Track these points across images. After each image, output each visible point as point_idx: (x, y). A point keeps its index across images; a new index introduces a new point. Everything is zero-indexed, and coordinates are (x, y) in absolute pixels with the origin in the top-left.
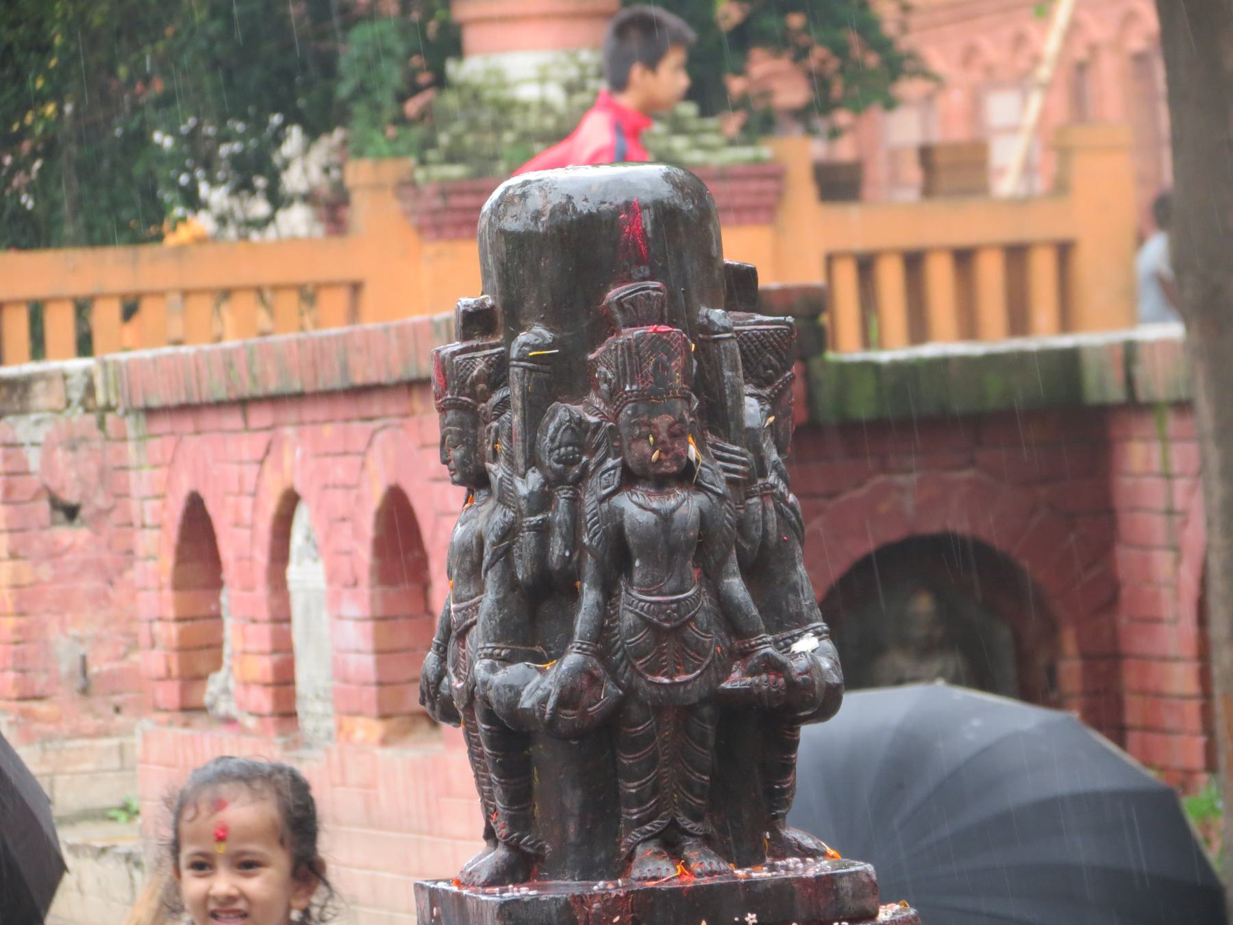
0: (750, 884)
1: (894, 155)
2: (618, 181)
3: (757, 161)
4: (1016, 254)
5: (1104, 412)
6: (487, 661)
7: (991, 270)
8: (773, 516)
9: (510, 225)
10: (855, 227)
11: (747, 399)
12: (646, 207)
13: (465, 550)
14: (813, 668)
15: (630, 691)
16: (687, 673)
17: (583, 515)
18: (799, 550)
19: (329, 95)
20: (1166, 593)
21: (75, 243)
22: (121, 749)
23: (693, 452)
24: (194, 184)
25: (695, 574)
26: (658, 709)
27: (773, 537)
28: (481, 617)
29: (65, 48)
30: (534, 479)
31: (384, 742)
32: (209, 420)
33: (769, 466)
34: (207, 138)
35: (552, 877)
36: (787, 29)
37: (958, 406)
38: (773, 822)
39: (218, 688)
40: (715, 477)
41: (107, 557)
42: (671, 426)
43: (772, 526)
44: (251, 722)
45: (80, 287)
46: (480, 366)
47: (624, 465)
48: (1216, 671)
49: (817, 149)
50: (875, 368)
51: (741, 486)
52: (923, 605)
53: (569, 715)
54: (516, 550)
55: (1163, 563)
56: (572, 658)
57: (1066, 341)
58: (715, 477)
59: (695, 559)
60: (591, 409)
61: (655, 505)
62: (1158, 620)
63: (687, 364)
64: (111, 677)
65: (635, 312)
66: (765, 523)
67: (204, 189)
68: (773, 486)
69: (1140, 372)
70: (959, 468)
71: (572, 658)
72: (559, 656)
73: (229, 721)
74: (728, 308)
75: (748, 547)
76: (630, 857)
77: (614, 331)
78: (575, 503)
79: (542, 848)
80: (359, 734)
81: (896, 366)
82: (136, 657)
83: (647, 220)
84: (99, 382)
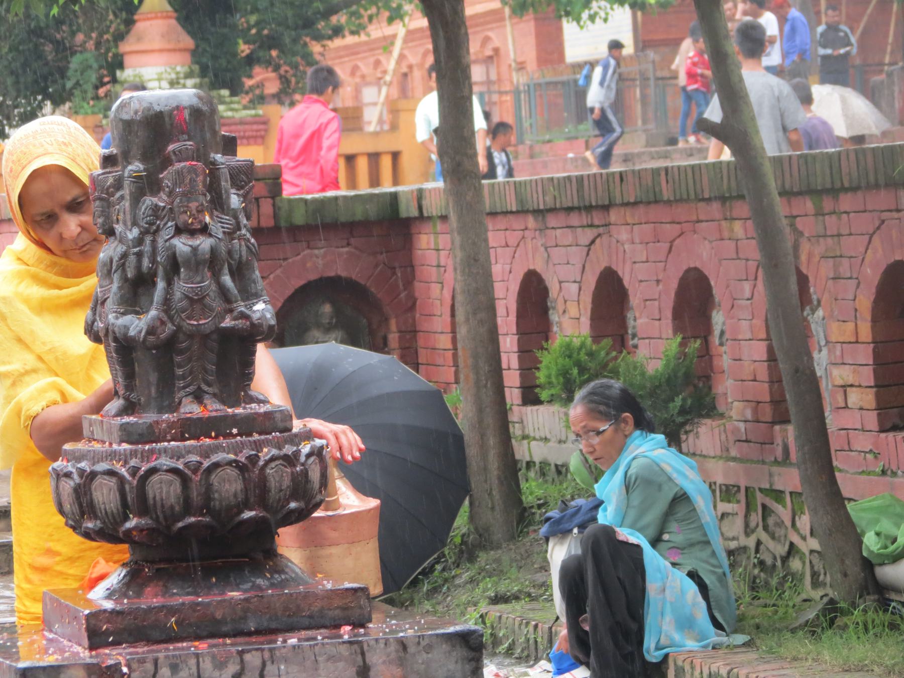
0: (234, 415)
2: (174, 97)
3: (256, 116)
4: (374, 158)
6: (114, 314)
7: (362, 165)
8: (244, 248)
9: (126, 117)
11: (232, 196)
12: (186, 108)
13: (105, 265)
14: (263, 317)
15: (179, 328)
18: (256, 264)
19: (64, 86)
23: (208, 219)
25: (209, 274)
26: (191, 336)
27: (244, 258)
28: (111, 295)
30: (135, 232)
34: (8, 106)
35: (144, 413)
36: (271, 56)
37: (343, 219)
40: (217, 230)
42: (197, 207)
43: (244, 253)
46: (111, 181)
47: (176, 225)
48: (458, 336)
50: (306, 201)
52: (327, 308)
53: (151, 338)
54: (127, 264)
55: (435, 289)
56: (153, 313)
58: (217, 230)
59: (209, 268)
60: (161, 200)
61: (190, 243)
63: (205, 180)
65: (181, 156)
71: (153, 313)
72: (147, 312)
74: (224, 154)
75: (233, 262)
76: (180, 403)
78: (154, 242)
79: (139, 400)
81: (314, 201)
83: (186, 114)
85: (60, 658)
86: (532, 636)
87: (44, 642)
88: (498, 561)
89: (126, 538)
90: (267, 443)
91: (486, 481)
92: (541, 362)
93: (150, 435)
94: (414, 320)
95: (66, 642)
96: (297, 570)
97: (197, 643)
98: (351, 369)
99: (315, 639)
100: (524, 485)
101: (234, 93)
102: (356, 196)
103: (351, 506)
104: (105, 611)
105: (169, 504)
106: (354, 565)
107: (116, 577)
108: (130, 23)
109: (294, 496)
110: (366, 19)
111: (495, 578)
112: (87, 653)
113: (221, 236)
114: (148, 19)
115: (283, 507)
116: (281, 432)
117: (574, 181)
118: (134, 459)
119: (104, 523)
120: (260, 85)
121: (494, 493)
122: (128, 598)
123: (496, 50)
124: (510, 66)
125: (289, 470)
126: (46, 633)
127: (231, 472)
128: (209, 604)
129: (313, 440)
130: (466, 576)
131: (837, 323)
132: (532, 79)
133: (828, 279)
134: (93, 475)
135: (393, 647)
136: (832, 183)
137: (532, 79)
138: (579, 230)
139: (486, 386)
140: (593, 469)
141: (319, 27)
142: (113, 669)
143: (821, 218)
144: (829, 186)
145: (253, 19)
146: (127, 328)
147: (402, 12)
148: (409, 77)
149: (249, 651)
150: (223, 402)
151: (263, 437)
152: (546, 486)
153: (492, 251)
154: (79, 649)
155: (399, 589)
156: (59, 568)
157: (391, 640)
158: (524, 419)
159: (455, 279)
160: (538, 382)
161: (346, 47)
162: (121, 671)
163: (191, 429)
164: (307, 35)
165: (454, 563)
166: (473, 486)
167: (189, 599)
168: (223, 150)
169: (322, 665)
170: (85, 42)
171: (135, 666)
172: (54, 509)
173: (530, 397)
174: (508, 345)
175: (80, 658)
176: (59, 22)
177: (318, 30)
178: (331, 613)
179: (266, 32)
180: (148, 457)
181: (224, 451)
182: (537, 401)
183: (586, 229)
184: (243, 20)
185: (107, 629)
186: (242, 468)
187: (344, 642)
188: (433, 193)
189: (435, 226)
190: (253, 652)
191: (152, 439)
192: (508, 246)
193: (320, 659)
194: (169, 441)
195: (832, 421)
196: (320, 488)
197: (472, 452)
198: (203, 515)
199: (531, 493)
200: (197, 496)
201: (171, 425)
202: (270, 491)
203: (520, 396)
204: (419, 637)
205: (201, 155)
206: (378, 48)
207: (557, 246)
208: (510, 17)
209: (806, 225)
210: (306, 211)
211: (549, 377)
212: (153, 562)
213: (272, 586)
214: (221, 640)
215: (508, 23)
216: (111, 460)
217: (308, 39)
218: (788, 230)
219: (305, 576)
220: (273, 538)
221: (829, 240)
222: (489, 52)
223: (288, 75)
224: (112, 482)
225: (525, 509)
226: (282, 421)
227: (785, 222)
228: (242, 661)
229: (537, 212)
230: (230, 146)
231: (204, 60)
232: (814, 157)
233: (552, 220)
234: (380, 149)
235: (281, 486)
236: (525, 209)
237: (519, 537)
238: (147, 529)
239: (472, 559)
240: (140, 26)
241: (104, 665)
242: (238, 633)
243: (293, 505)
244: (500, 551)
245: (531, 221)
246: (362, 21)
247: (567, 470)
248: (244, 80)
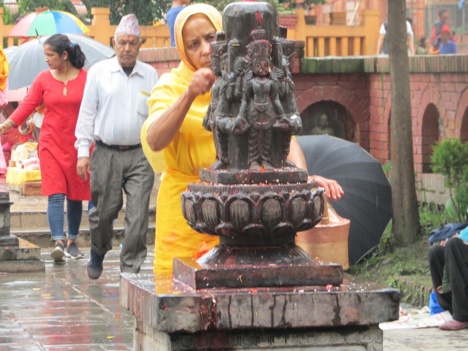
1: (324, 15)
2: (256, 6)
3: (292, 14)
4: (351, 39)
5: (369, 74)
7: (345, 42)
8: (288, 87)
9: (230, 15)
10: (313, 31)
14: (295, 123)
15: (252, 126)
17: (243, 83)
20: (381, 117)
23: (270, 70)
24: (160, 12)
26: (258, 130)
27: (287, 92)
28: (218, 107)
33: (287, 75)
37: (335, 71)
40: (275, 76)
43: (288, 89)
46: (221, 48)
48: (392, 136)
49: (306, 12)
50: (316, 61)
51: (281, 79)
52: (324, 117)
53: (237, 130)
54: (227, 91)
55: (381, 110)
56: (239, 117)
57: (361, 57)
58: (275, 76)
59: (269, 96)
60: (246, 59)
62: (379, 123)
65: (258, 37)
66: (286, 88)
67: (162, 14)
69: (378, 65)
70: (334, 85)
72: (236, 116)
74: (280, 37)
75: (281, 93)
76: (250, 164)
78: (241, 81)
81: (320, 61)
83: (262, 15)
85: (181, 293)
86: (421, 293)
87: (173, 284)
88: (405, 253)
89: (219, 233)
91: (401, 211)
93: (234, 180)
94: (369, 125)
95: (184, 285)
96: (306, 255)
97: (252, 289)
98: (335, 149)
99: (313, 291)
100: (421, 215)
103: (335, 223)
104: (205, 270)
105: (242, 216)
106: (335, 254)
107: (212, 252)
111: (403, 262)
112: (195, 291)
113: (276, 79)
115: (300, 221)
116: (301, 182)
117: (456, 59)
118: (225, 192)
119: (207, 224)
122: (218, 263)
125: (304, 203)
126: (174, 279)
127: (275, 202)
128: (260, 269)
129: (318, 188)
130: (388, 260)
134: (203, 199)
135: (353, 298)
140: (458, 208)
142: (208, 300)
146: (225, 124)
149: (279, 295)
150: (273, 166)
151: (292, 185)
153: (411, 93)
154: (190, 288)
156: (178, 243)
157: (352, 294)
158: (423, 180)
160: (431, 162)
162: (212, 301)
163: (255, 178)
166: (395, 213)
167: (249, 266)
169: (316, 305)
171: (219, 299)
172: (182, 217)
173: (427, 169)
175: (191, 293)
178: (322, 278)
180: (232, 192)
181: (272, 191)
182: (430, 171)
185: (206, 279)
186: (281, 200)
187: (328, 294)
190: (281, 296)
191: (235, 182)
193: (315, 302)
194: (243, 184)
197: (395, 196)
198: (258, 223)
201: (245, 176)
202: (294, 213)
204: (367, 293)
205: (268, 36)
210: (316, 66)
211: (437, 159)
212: (231, 246)
213: (293, 262)
214: (264, 289)
216: (213, 192)
219: (309, 258)
224: (213, 204)
225: (421, 227)
226: (302, 177)
228: (275, 300)
230: (283, 33)
233: (443, 78)
235: (300, 210)
239: (392, 251)
241: (203, 298)
242: (274, 286)
243: (305, 221)
244: (406, 248)
245: (432, 78)
247: (444, 208)
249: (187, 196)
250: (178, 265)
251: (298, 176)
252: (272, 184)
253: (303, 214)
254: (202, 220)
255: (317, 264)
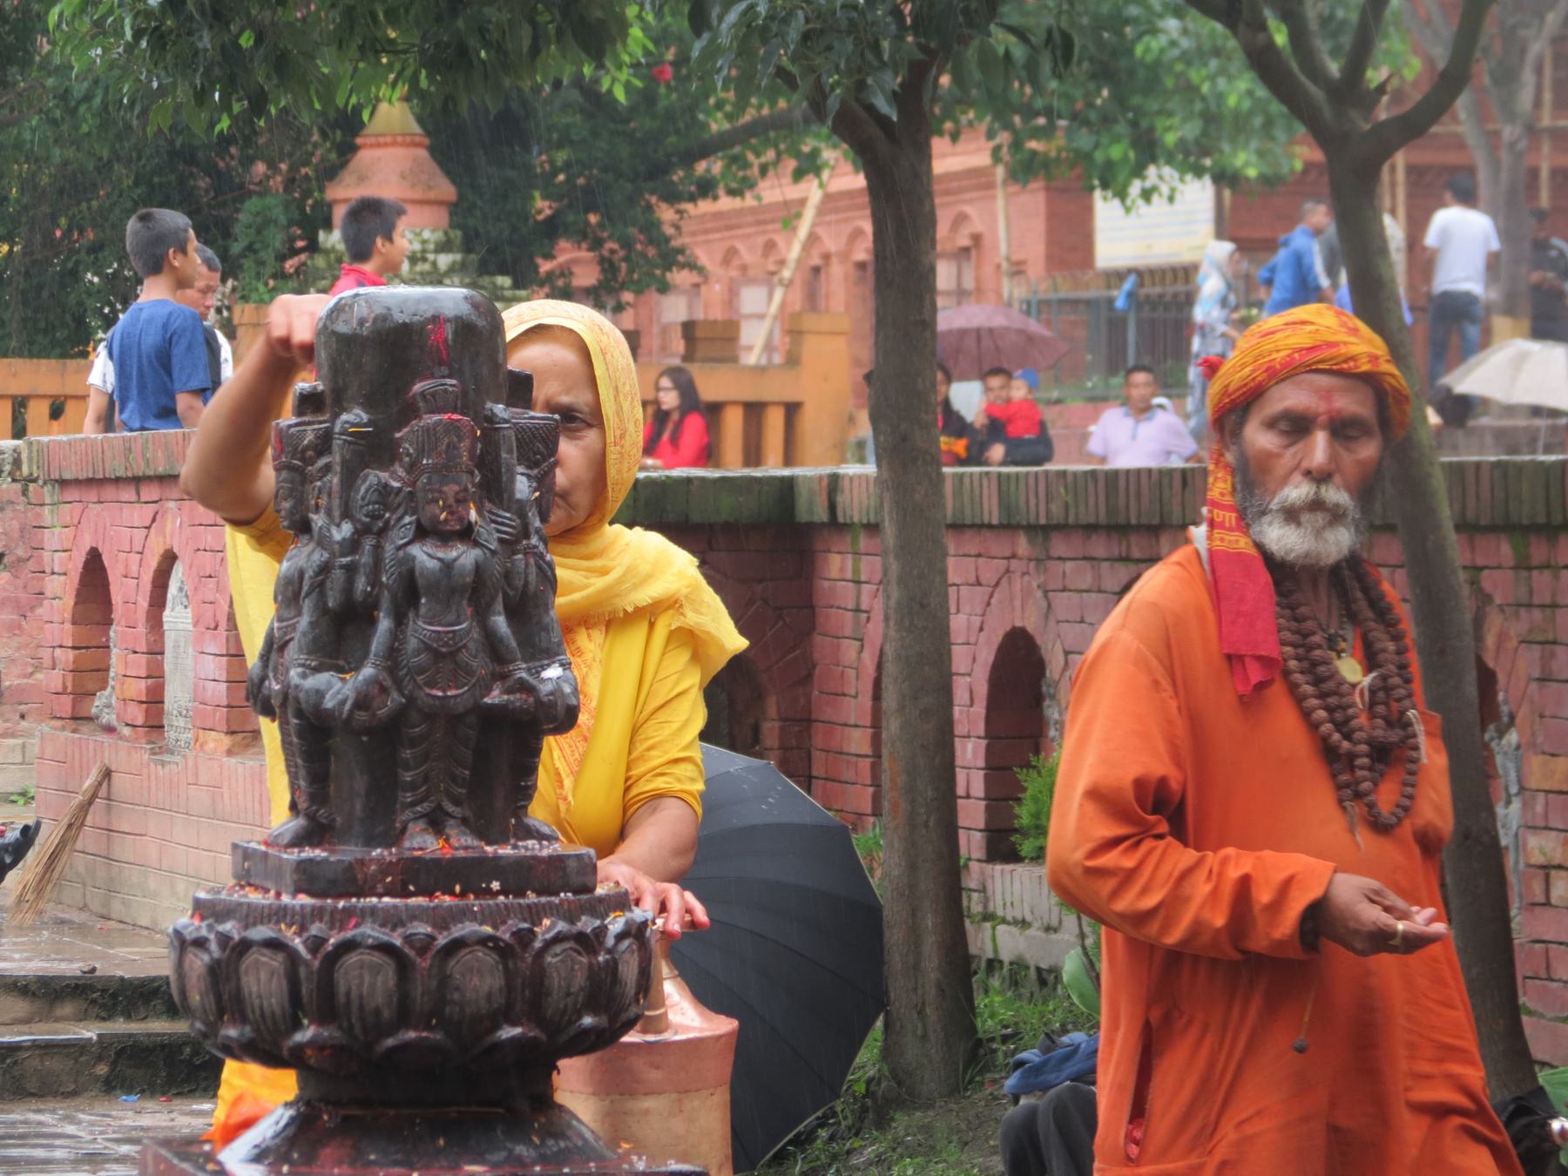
1: (665, 330)
2: (429, 299)
4: (754, 411)
5: (811, 527)
6: (300, 670)
8: (533, 570)
9: (342, 328)
12: (449, 320)
15: (411, 700)
16: (458, 688)
21: (18, 353)
22: (24, 746)
23: (473, 515)
25: (469, 611)
26: (430, 716)
27: (532, 587)
28: (297, 635)
29: (18, 201)
30: (347, 529)
31: (230, 753)
32: (110, 492)
33: (532, 531)
34: (126, 279)
36: (587, 223)
38: (520, 810)
39: (104, 704)
40: (490, 535)
41: (22, 595)
43: (533, 577)
44: (126, 731)
45: (17, 388)
46: (309, 437)
51: (509, 545)
53: (362, 716)
54: (328, 583)
55: (849, 650)
56: (368, 671)
57: (786, 472)
59: (470, 599)
61: (440, 554)
64: (21, 690)
65: (436, 402)
66: (526, 576)
68: (535, 547)
71: (368, 671)
72: (357, 669)
73: (110, 729)
74: (508, 405)
75: (511, 593)
76: (403, 830)
77: (418, 417)
78: (378, 548)
79: (334, 820)
80: (211, 745)
82: (39, 676)
83: (449, 331)
84: (24, 456)
88: (927, 1129)
90: (549, 910)
91: (915, 989)
92: (1024, 790)
93: (350, 882)
94: (809, 701)
96: (588, 1135)
100: (981, 1002)
101: (517, 285)
102: (723, 479)
103: (688, 1029)
108: (347, 150)
109: (591, 1005)
110: (756, 170)
114: (379, 145)
115: (570, 1023)
116: (575, 892)
119: (257, 1030)
120: (566, 272)
121: (928, 1010)
123: (977, 238)
124: (999, 266)
125: (584, 960)
130: (870, 1152)
131: (1540, 758)
132: (1035, 292)
133: (1530, 679)
134: (245, 946)
136: (1548, 515)
137: (1035, 292)
138: (1105, 565)
139: (926, 825)
141: (675, 178)
143: (1524, 574)
144: (1541, 519)
145: (561, 156)
146: (320, 694)
147: (819, 162)
148: (823, 275)
151: (543, 899)
152: (1018, 1004)
153: (952, 590)
155: (753, 1168)
159: (885, 636)
160: (1016, 824)
161: (718, 215)
164: (653, 192)
165: (849, 1128)
168: (510, 396)
170: (268, 178)
174: (969, 754)
176: (225, 140)
177: (672, 182)
179: (581, 181)
180: (341, 921)
182: (1013, 857)
183: (1116, 564)
184: (544, 157)
186: (504, 952)
188: (856, 483)
189: (855, 541)
192: (979, 584)
194: (380, 896)
195: (1522, 925)
196: (637, 994)
197: (894, 935)
199: (992, 1016)
200: (423, 995)
201: (386, 868)
202: (549, 994)
203: (984, 845)
206: (772, 221)
207: (1064, 590)
208: (1005, 182)
209: (1499, 585)
212: (337, 1104)
213: (543, 1159)
215: (1000, 193)
216: (278, 922)
217: (654, 200)
218: (1466, 591)
219: (600, 1146)
220: (550, 1075)
221: (1537, 614)
222: (964, 241)
223: (616, 258)
224: (277, 961)
225: (979, 1043)
227: (1462, 576)
229: (1032, 529)
231: (471, 222)
232: (1520, 467)
233: (1059, 546)
234: (765, 396)
235: (569, 986)
236: (1014, 522)
237: (966, 1089)
238: (333, 1047)
239: (882, 1123)
240: (364, 157)
243: (588, 1020)
244: (931, 1113)
245: (1023, 545)
246: (749, 173)
247: (1058, 979)
248: (539, 261)
249: (190, 934)
250: (157, 1165)
251: (564, 869)
252: (477, 897)
253: (580, 999)
254: (241, 1017)
255: (626, 1166)
